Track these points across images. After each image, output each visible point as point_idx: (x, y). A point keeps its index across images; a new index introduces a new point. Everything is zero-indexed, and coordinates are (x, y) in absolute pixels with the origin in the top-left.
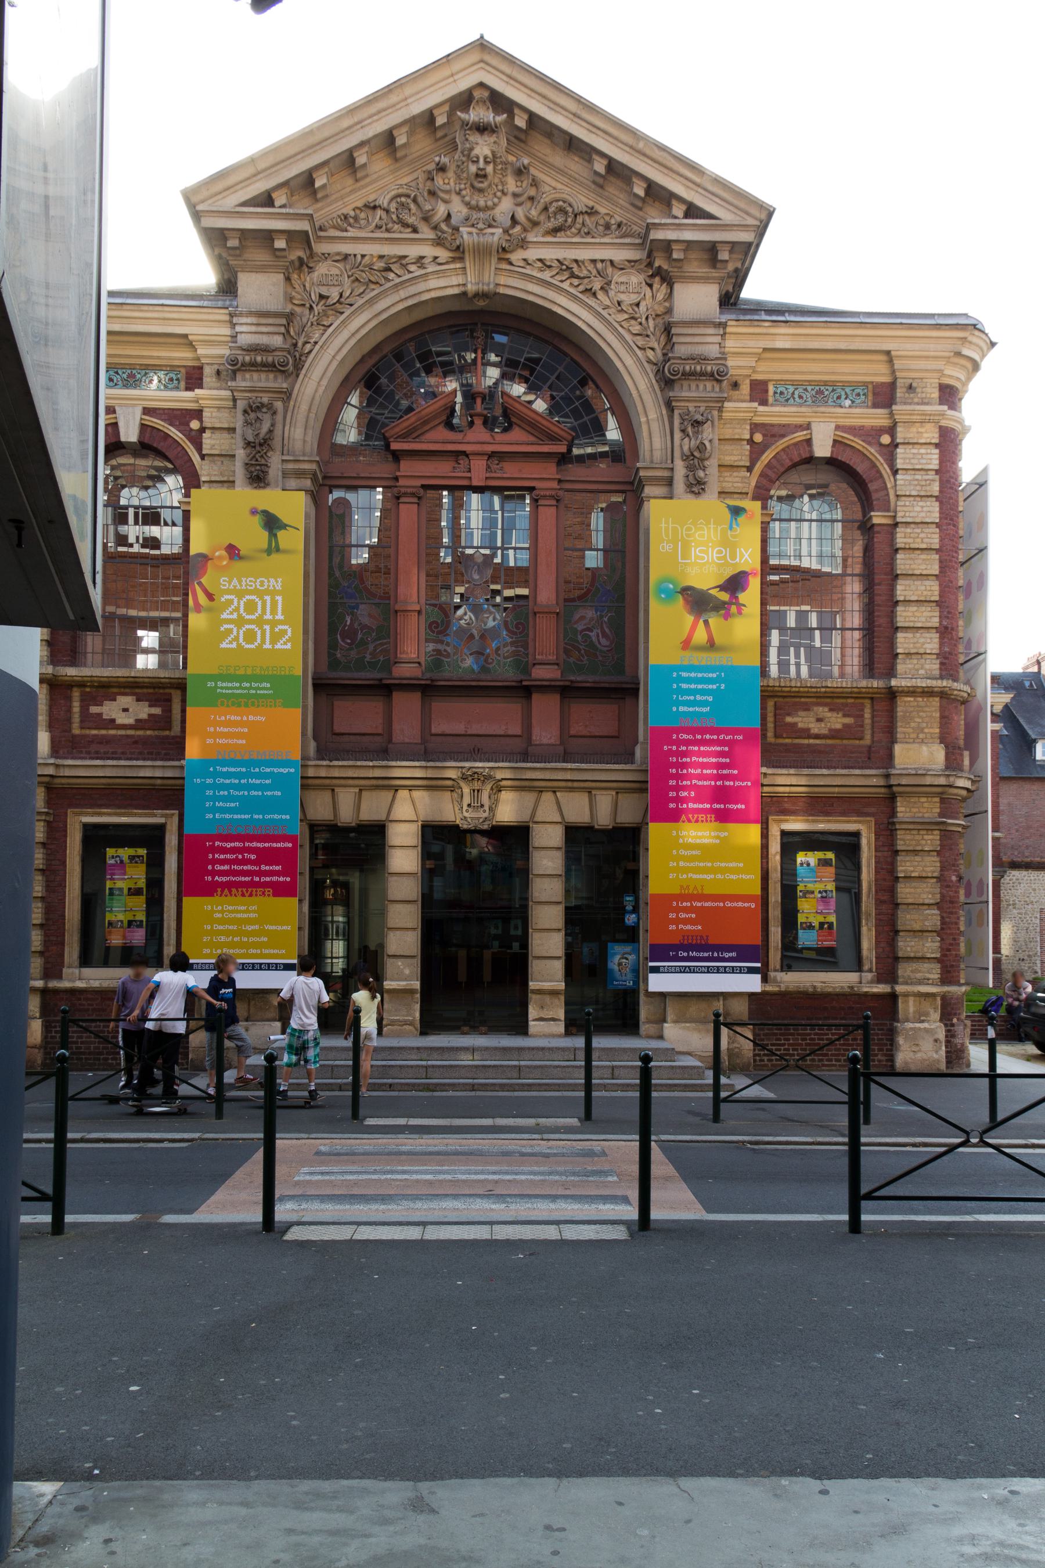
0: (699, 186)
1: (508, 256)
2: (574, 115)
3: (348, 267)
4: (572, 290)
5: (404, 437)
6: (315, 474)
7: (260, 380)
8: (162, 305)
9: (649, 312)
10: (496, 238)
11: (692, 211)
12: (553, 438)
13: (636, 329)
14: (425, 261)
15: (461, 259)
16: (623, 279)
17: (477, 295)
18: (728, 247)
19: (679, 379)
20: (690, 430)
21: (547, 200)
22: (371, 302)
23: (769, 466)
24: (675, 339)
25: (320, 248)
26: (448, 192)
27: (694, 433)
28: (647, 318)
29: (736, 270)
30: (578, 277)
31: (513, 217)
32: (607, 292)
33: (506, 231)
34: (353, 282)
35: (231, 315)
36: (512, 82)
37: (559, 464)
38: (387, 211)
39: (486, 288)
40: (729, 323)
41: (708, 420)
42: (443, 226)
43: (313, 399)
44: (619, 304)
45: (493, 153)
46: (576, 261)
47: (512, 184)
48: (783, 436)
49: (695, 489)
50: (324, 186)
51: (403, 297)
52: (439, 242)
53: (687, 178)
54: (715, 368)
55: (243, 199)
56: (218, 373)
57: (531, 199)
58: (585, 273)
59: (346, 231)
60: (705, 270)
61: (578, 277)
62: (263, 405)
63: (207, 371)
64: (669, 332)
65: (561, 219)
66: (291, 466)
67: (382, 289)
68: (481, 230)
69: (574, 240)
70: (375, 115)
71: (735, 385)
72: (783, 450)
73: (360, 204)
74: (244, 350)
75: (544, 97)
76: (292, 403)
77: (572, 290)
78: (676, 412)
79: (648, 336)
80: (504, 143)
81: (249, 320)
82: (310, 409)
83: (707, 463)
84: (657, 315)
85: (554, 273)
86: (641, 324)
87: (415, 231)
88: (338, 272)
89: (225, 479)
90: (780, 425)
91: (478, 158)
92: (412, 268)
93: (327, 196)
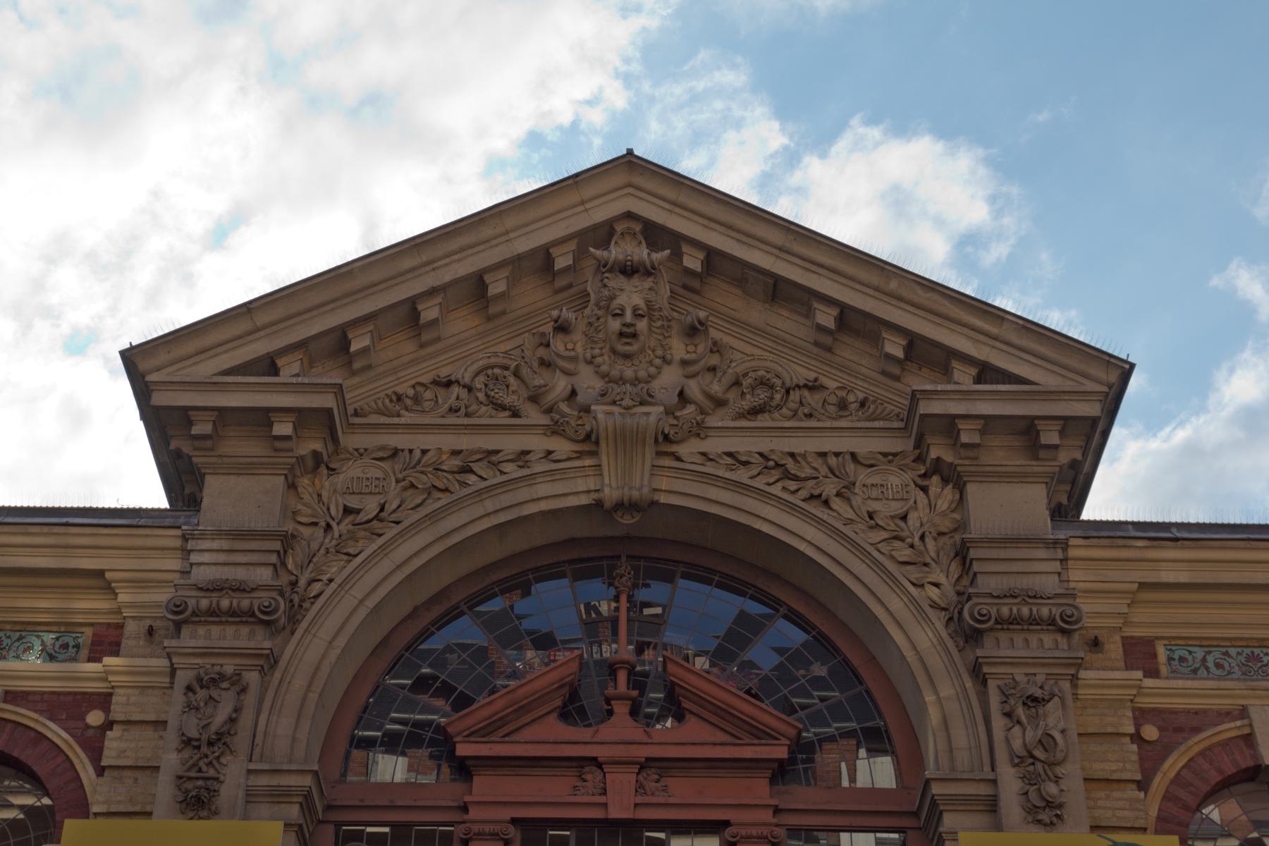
0: (996, 339)
1: (673, 448)
2: (780, 249)
3: (397, 467)
4: (786, 496)
5: (484, 732)
6: (308, 796)
7: (225, 638)
8: (67, 525)
9: (926, 528)
10: (652, 419)
11: (986, 372)
12: (761, 734)
13: (904, 553)
14: (531, 457)
15: (593, 454)
16: (876, 479)
17: (619, 506)
18: (1057, 426)
19: (991, 629)
20: (1020, 712)
21: (739, 370)
22: (433, 517)
23: (1177, 780)
24: (976, 567)
25: (351, 441)
26: (574, 359)
27: (1029, 717)
28: (922, 538)
29: (1074, 465)
30: (796, 478)
31: (681, 394)
32: (848, 500)
33: (669, 412)
34: (405, 489)
35: (185, 538)
36: (677, 210)
37: (773, 781)
38: (470, 389)
39: (636, 494)
40: (1073, 542)
41: (1053, 696)
42: (564, 407)
43: (318, 668)
44: (871, 518)
45: (648, 302)
46: (792, 455)
47: (679, 348)
48: (1197, 730)
49: (1044, 817)
50: (365, 351)
51: (491, 509)
52: (555, 430)
53: (974, 329)
54: (1056, 612)
55: (227, 366)
56: (151, 631)
57: (713, 369)
58: (808, 471)
59: (399, 416)
60: (1018, 462)
61: (796, 478)
62: (222, 677)
63: (131, 627)
64: (964, 559)
65: (762, 395)
66: (263, 781)
67: (454, 497)
68: (628, 408)
69: (787, 424)
70: (456, 253)
71: (1096, 644)
72: (1202, 753)
73: (426, 379)
74: (201, 589)
75: (731, 227)
76: (278, 675)
77: (786, 496)
78: (992, 684)
79: (926, 565)
80: (665, 291)
81: (215, 545)
82: (309, 686)
83: (1059, 770)
84: (941, 534)
85: (755, 472)
86: (912, 546)
87: (516, 414)
88: (380, 474)
89: (137, 808)
90: (1188, 712)
91: (623, 309)
92: (509, 467)
93: (369, 367)
